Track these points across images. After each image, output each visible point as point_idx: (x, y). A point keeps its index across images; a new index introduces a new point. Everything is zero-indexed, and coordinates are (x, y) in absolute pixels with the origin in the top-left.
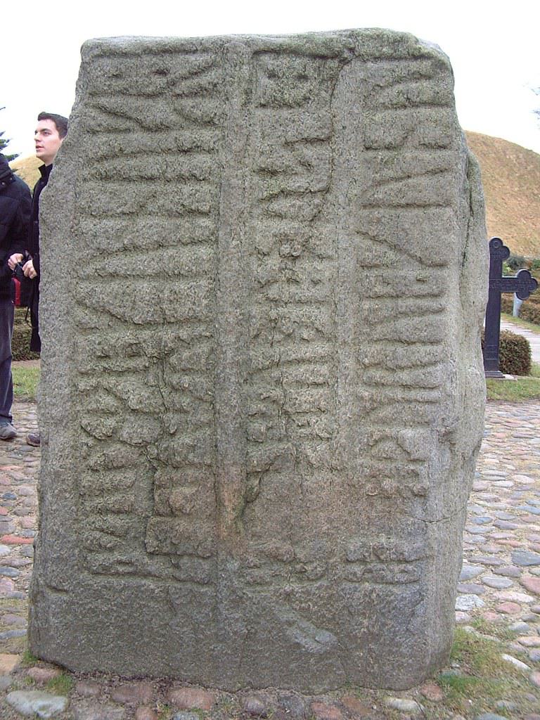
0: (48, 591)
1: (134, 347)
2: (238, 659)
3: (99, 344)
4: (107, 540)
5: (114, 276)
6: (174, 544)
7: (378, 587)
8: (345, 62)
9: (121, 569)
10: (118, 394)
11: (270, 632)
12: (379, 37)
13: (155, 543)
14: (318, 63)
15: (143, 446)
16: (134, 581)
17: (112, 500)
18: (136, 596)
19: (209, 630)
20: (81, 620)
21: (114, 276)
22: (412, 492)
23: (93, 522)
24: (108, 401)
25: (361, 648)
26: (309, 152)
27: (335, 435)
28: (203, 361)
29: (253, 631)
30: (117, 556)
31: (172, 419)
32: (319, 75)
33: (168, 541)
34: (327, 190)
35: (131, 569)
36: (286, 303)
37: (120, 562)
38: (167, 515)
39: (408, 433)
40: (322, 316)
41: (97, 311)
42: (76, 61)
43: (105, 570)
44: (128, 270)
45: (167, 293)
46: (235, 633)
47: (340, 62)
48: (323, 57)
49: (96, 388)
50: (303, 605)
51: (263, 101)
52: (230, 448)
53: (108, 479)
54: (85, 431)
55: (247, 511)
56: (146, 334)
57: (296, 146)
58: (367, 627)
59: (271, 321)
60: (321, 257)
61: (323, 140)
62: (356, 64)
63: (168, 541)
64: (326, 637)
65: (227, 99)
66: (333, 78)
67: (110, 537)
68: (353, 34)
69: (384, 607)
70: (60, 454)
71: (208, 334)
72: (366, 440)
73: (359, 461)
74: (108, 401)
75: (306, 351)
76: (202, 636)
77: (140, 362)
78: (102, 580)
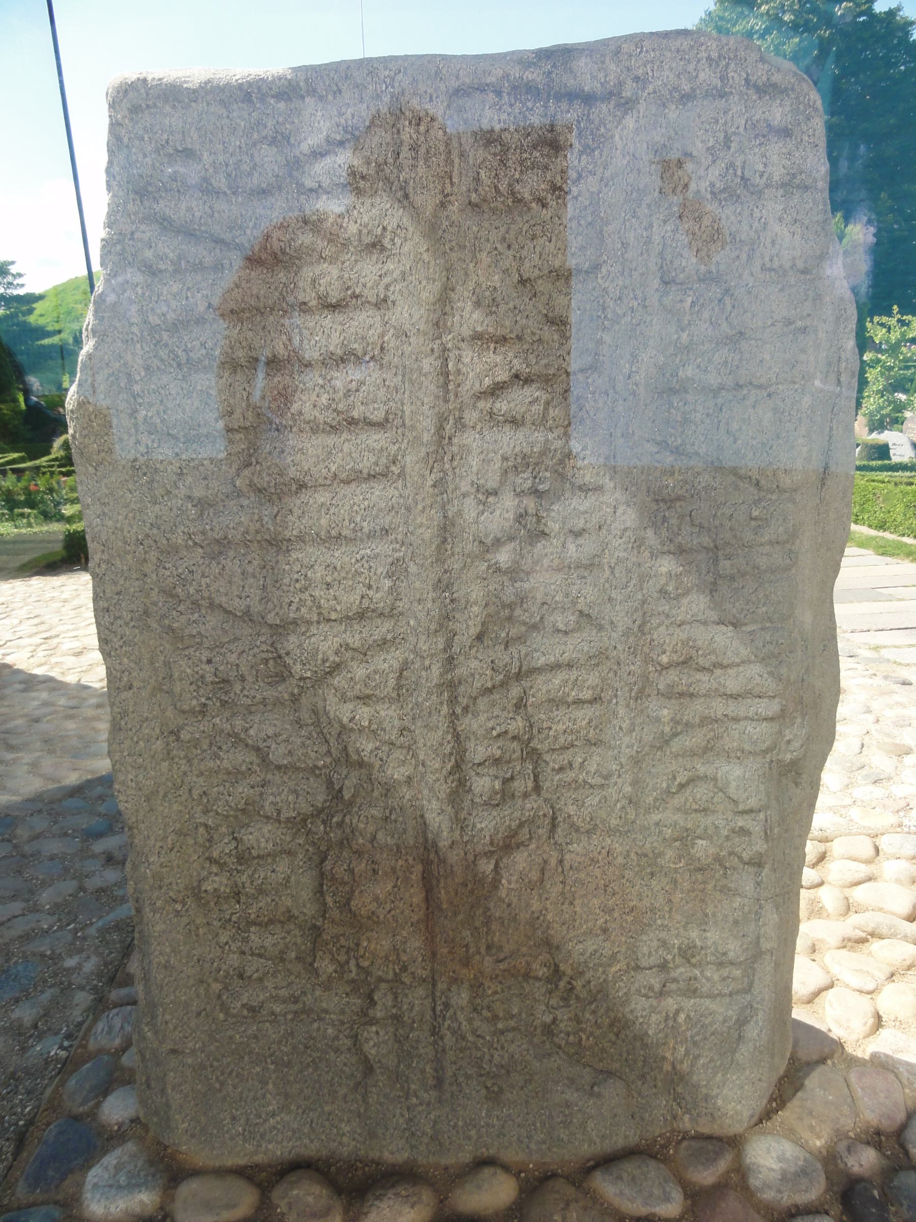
3: (209, 661)
10: (250, 742)
15: (299, 824)
24: (240, 758)
69: (698, 1034)
74: (240, 758)
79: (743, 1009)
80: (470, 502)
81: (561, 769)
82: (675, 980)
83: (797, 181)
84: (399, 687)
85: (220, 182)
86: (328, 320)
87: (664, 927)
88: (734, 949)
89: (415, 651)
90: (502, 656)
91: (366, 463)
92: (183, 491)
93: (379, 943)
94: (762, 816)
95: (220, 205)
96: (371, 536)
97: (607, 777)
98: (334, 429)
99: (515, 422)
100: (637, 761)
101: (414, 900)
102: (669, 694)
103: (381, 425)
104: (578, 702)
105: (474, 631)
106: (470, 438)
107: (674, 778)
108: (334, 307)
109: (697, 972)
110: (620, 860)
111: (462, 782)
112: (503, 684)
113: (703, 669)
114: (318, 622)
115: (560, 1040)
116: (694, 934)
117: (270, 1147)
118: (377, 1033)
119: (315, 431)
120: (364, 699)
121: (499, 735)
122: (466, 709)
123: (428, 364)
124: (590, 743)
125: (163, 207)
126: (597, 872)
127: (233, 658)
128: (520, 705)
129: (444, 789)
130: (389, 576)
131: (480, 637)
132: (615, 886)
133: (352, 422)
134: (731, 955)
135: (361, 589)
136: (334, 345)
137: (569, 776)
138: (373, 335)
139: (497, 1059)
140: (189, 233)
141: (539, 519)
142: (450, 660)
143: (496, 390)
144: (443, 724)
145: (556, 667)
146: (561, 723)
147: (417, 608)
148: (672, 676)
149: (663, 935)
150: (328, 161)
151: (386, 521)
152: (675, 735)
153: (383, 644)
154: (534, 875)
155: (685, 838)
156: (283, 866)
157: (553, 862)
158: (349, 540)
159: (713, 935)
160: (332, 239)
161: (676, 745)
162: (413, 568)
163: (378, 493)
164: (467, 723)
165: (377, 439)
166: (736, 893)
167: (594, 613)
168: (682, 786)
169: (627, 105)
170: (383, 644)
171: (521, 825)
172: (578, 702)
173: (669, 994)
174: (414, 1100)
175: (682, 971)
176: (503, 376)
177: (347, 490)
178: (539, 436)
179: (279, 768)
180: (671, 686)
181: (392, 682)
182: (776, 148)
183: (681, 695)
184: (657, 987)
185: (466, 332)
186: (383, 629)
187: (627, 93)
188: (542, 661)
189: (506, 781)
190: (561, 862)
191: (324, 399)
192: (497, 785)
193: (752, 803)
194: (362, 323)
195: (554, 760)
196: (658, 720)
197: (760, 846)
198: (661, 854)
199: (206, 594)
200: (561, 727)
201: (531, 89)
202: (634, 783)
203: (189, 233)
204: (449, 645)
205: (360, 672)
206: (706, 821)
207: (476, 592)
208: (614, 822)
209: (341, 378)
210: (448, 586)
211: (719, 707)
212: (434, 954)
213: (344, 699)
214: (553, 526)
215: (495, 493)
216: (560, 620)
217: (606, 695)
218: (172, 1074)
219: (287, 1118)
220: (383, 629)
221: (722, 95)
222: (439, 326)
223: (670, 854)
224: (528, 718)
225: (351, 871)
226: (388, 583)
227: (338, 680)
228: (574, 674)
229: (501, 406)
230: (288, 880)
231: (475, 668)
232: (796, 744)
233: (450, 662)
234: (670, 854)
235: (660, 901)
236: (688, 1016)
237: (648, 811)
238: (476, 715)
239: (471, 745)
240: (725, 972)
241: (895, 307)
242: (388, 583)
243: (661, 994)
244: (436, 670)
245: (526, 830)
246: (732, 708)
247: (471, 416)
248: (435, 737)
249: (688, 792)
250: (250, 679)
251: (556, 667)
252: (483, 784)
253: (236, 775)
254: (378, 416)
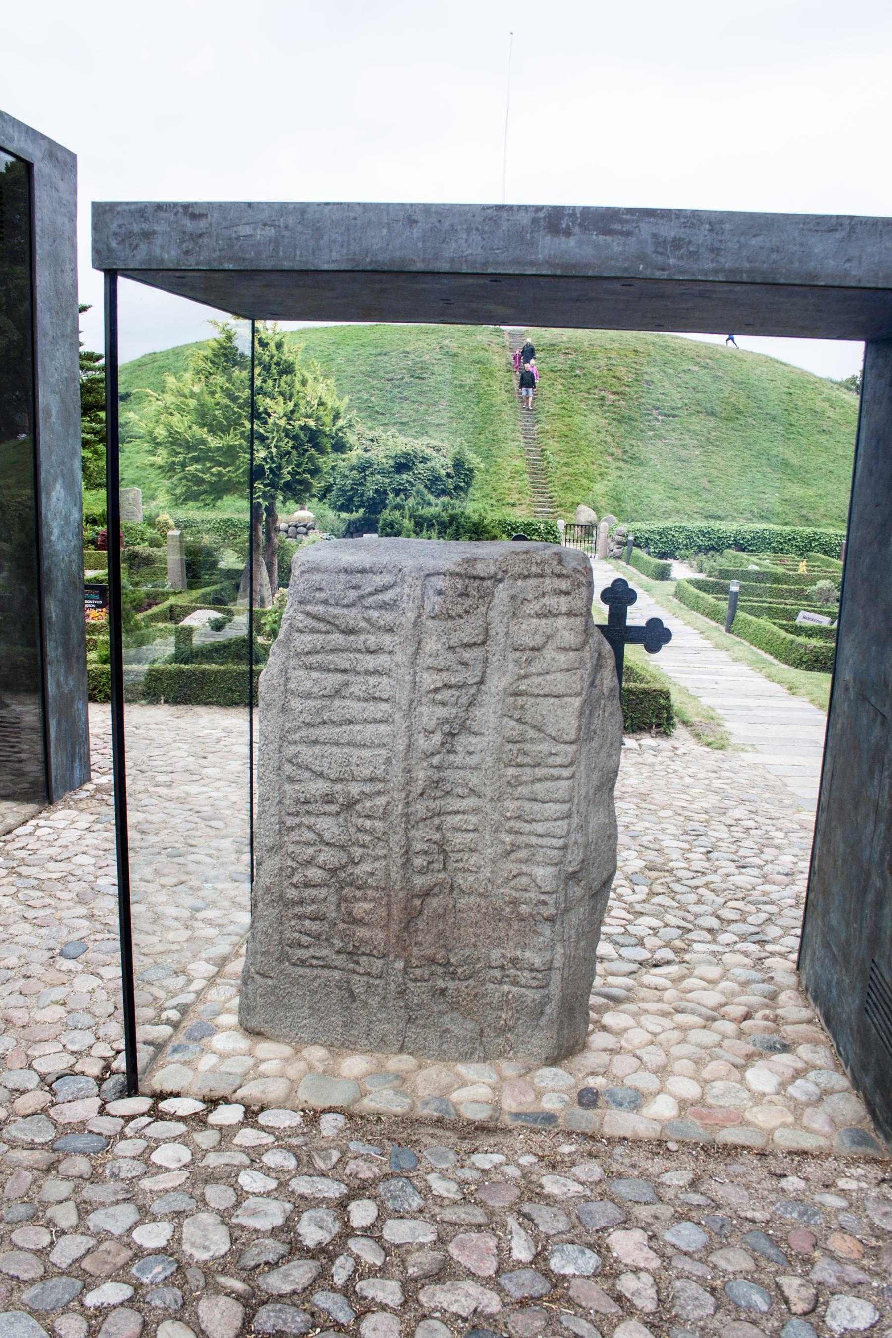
24: (309, 836)
74: (309, 836)
79: (544, 997)
80: (422, 735)
81: (457, 861)
82: (508, 976)
84: (384, 813)
85: (332, 601)
86: (369, 657)
87: (504, 948)
88: (537, 961)
89: (392, 798)
90: (431, 804)
91: (379, 716)
92: (302, 719)
94: (554, 896)
95: (330, 609)
96: (378, 746)
97: (479, 868)
98: (367, 700)
99: (443, 704)
100: (493, 862)
102: (510, 831)
103: (386, 701)
104: (468, 830)
105: (419, 792)
106: (424, 709)
108: (371, 652)
109: (519, 973)
110: (484, 910)
111: (408, 860)
112: (431, 817)
113: (526, 821)
116: (519, 953)
119: (359, 700)
120: (368, 817)
122: (413, 826)
123: (408, 678)
124: (472, 851)
125: (309, 608)
126: (472, 915)
129: (400, 861)
130: (384, 764)
131: (422, 795)
132: (481, 923)
133: (375, 698)
134: (536, 965)
135: (371, 768)
136: (370, 667)
137: (461, 865)
138: (386, 665)
139: (415, 1001)
140: (315, 618)
141: (442, 744)
142: (408, 803)
143: (436, 690)
144: (402, 832)
145: (457, 812)
146: (458, 839)
147: (395, 779)
148: (512, 823)
149: (503, 951)
150: (375, 597)
151: (385, 740)
152: (513, 851)
153: (379, 793)
154: (441, 911)
155: (515, 903)
156: (324, 891)
157: (451, 906)
158: (369, 747)
159: (528, 954)
160: (372, 625)
161: (513, 856)
162: (394, 762)
163: (383, 728)
164: (413, 833)
165: (384, 706)
166: (541, 934)
167: (477, 789)
168: (515, 877)
169: (500, 581)
170: (379, 793)
171: (435, 885)
172: (468, 830)
173: (505, 982)
175: (512, 972)
176: (439, 685)
177: (369, 726)
178: (454, 710)
179: (328, 844)
180: (511, 828)
181: (381, 811)
182: (563, 599)
183: (516, 832)
184: (499, 978)
185: (425, 666)
186: (380, 786)
187: (499, 577)
188: (451, 809)
189: (429, 863)
190: (455, 907)
191: (364, 688)
192: (425, 864)
193: (548, 889)
194: (383, 660)
195: (454, 856)
196: (504, 843)
197: (552, 911)
198: (503, 910)
200: (458, 841)
201: (459, 575)
202: (492, 872)
203: (315, 618)
204: (407, 796)
205: (368, 804)
206: (527, 895)
207: (421, 774)
208: (481, 890)
209: (372, 680)
210: (409, 771)
211: (534, 840)
213: (360, 816)
214: (459, 749)
215: (433, 733)
216: (460, 791)
217: (480, 829)
220: (380, 786)
221: (542, 576)
222: (413, 664)
223: (508, 910)
224: (443, 835)
226: (383, 767)
227: (358, 807)
228: (466, 817)
229: (438, 697)
230: (326, 898)
231: (419, 808)
232: (574, 863)
233: (408, 804)
234: (508, 910)
235: (503, 934)
237: (498, 887)
238: (418, 830)
239: (414, 843)
240: (534, 974)
242: (383, 767)
243: (501, 982)
244: (400, 807)
245: (437, 888)
246: (541, 841)
247: (424, 700)
248: (397, 837)
249: (518, 879)
251: (457, 812)
252: (419, 862)
253: (308, 844)
254: (386, 697)
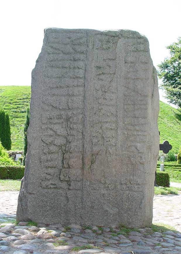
0: (28, 195)
1: (59, 116)
2: (88, 215)
3: (49, 115)
4: (48, 177)
5: (54, 95)
6: (69, 177)
7: (131, 192)
8: (120, 38)
9: (52, 186)
10: (54, 130)
11: (98, 206)
12: (129, 32)
13: (63, 177)
14: (112, 38)
15: (60, 147)
16: (56, 190)
17: (50, 164)
18: (56, 196)
19: (80, 205)
20: (38, 204)
21: (54, 95)
22: (140, 163)
23: (44, 171)
24: (51, 132)
25: (126, 213)
26: (110, 63)
27: (117, 144)
28: (80, 120)
29: (93, 205)
30: (51, 182)
31: (70, 138)
32: (113, 41)
33: (68, 176)
34: (114, 74)
35: (55, 186)
36: (103, 105)
37: (52, 184)
38: (67, 168)
39: (138, 145)
40: (113, 110)
41: (48, 105)
42: (42, 36)
43: (47, 187)
44: (58, 93)
45: (70, 100)
46: (88, 206)
47: (118, 38)
48: (114, 37)
49: (47, 128)
50: (108, 198)
51: (97, 48)
52: (88, 147)
53: (49, 157)
54: (43, 141)
55: (92, 166)
56: (63, 112)
57: (107, 60)
58: (128, 206)
59: (99, 109)
60: (113, 93)
61: (114, 60)
62: (122, 39)
63: (68, 176)
64: (116, 210)
65: (88, 46)
66: (116, 42)
67: (49, 176)
68: (122, 31)
69: (132, 199)
70: (35, 148)
71: (81, 112)
72: (126, 146)
73: (124, 152)
74: (51, 132)
75: (109, 120)
76: (77, 208)
77: (61, 121)
78: (46, 190)
83: (145, 50)
93: (73, 171)
101: (81, 163)
107: (128, 145)
114: (68, 109)
115: (106, 198)
117: (47, 219)
118: (71, 192)
121: (97, 132)
127: (53, 114)
128: (101, 128)
156: (56, 155)
174: (77, 208)
199: (50, 103)
212: (83, 174)
218: (29, 199)
219: (51, 212)
225: (69, 156)
236: (131, 195)
241: (180, 86)
250: (55, 118)
253: (51, 136)
